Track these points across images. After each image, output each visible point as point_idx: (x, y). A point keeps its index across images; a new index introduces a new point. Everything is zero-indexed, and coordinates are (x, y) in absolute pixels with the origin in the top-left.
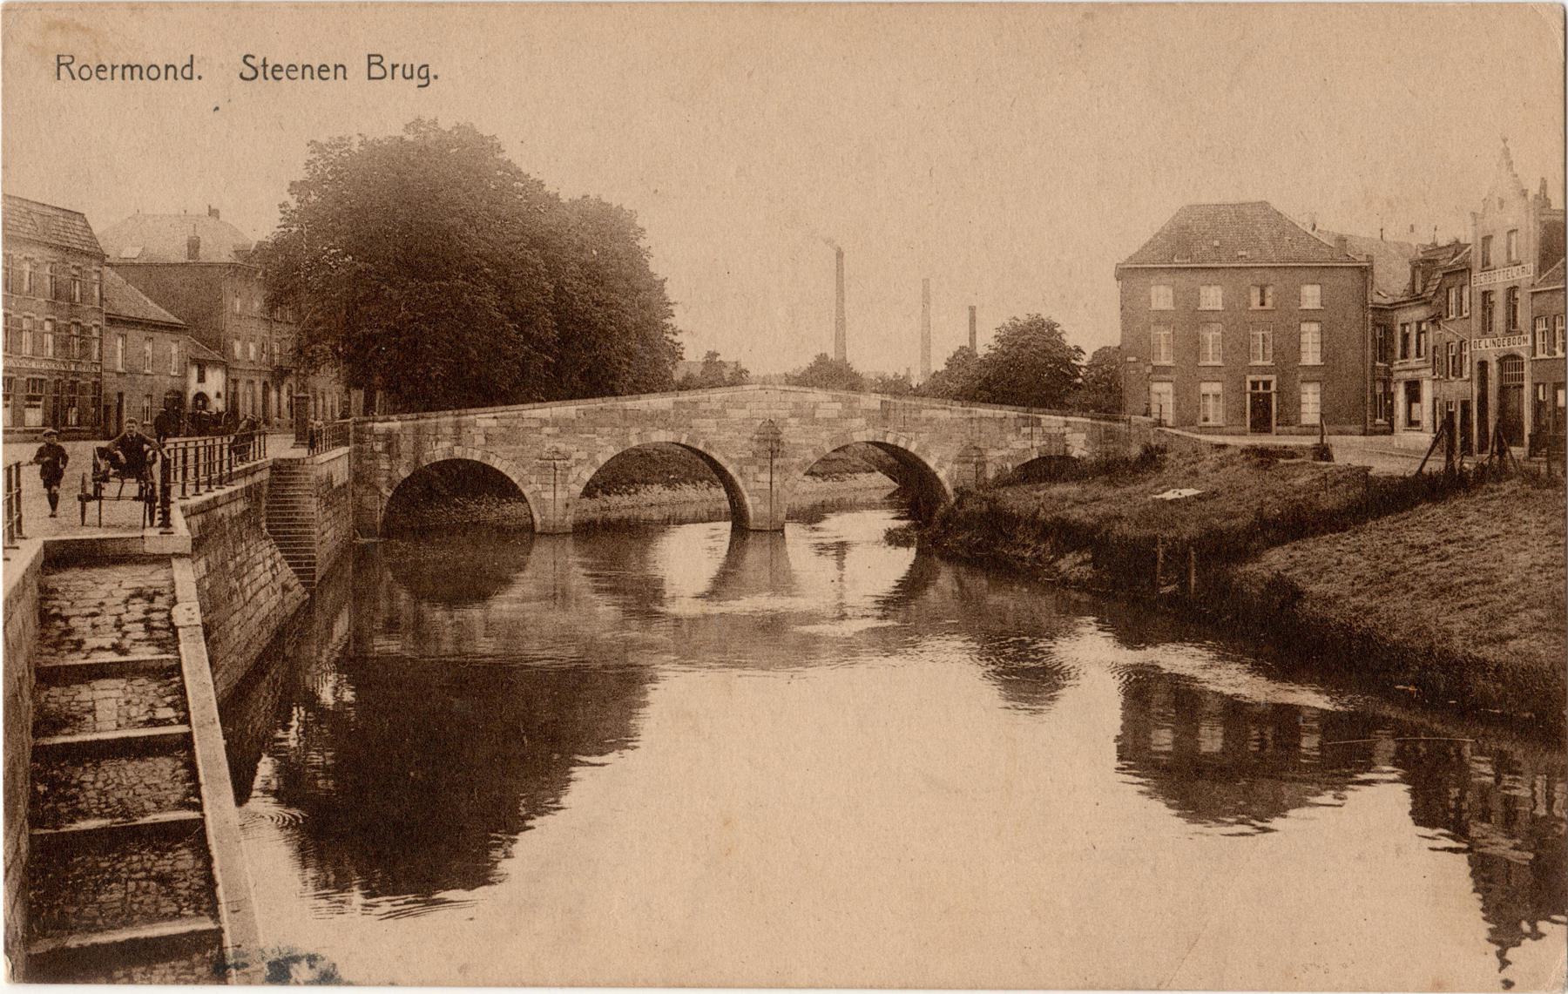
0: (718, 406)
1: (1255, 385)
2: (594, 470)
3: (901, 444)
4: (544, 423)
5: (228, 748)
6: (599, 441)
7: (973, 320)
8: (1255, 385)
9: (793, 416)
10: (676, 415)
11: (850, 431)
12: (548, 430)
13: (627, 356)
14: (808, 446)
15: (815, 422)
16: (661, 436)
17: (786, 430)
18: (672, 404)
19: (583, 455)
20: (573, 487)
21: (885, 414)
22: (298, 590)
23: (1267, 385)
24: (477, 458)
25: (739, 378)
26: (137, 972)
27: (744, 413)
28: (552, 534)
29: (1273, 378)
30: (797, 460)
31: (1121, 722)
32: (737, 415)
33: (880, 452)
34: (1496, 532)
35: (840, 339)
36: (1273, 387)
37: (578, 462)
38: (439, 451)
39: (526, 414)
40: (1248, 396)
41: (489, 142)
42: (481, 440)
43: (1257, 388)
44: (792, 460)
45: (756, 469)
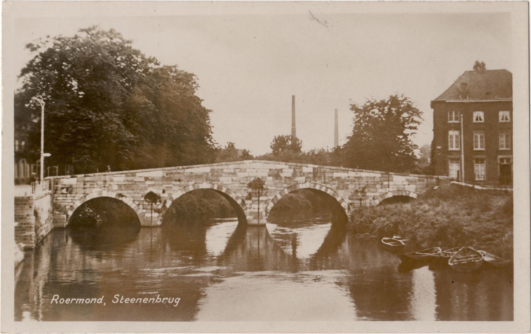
0: (232, 171)
1: (502, 160)
4: (147, 179)
7: (336, 117)
11: (297, 183)
12: (148, 183)
13: (121, 144)
16: (205, 185)
18: (210, 171)
21: (315, 174)
22: (477, 179)
25: (246, 156)
26: (288, 272)
28: (391, 192)
31: (435, 291)
32: (241, 175)
33: (310, 192)
35: (294, 131)
38: (94, 194)
40: (499, 166)
43: (503, 162)
45: (250, 202)
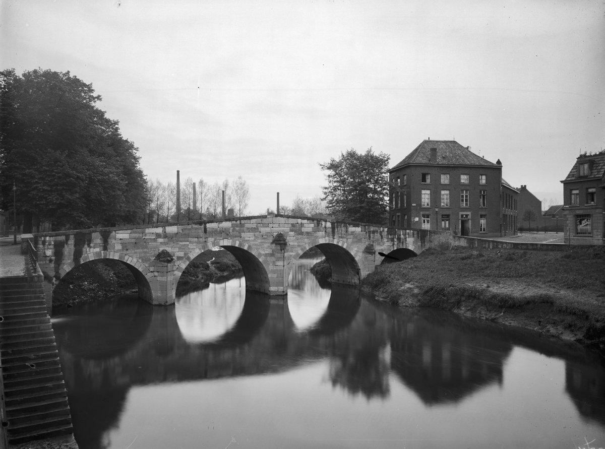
1: (462, 216)
2: (188, 263)
3: (340, 244)
5: (75, 252)
6: (191, 246)
8: (462, 216)
9: (291, 231)
10: (233, 231)
12: (160, 240)
14: (299, 246)
15: (302, 233)
17: (288, 238)
19: (182, 254)
20: (176, 272)
23: (467, 216)
24: (116, 258)
27: (268, 230)
29: (469, 213)
30: (293, 254)
34: (285, 267)
36: (469, 217)
37: (179, 258)
39: (147, 231)
40: (460, 221)
41: (72, 227)
42: (118, 247)
44: (291, 253)
